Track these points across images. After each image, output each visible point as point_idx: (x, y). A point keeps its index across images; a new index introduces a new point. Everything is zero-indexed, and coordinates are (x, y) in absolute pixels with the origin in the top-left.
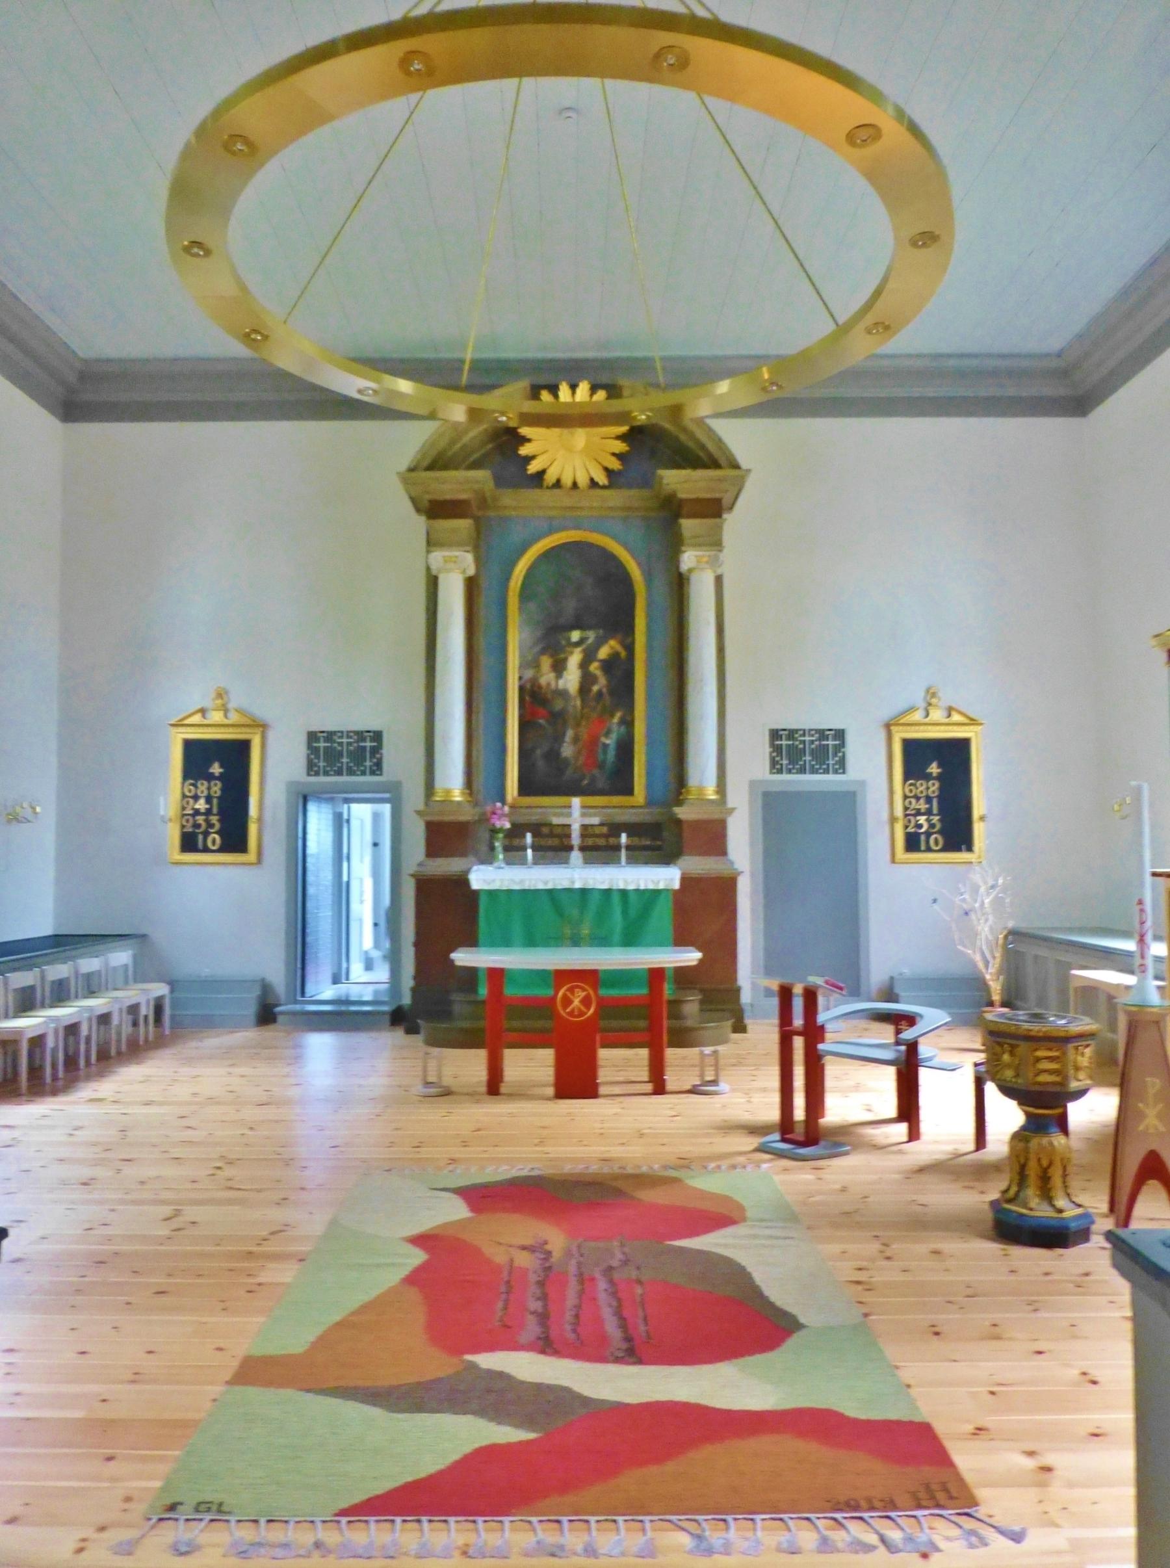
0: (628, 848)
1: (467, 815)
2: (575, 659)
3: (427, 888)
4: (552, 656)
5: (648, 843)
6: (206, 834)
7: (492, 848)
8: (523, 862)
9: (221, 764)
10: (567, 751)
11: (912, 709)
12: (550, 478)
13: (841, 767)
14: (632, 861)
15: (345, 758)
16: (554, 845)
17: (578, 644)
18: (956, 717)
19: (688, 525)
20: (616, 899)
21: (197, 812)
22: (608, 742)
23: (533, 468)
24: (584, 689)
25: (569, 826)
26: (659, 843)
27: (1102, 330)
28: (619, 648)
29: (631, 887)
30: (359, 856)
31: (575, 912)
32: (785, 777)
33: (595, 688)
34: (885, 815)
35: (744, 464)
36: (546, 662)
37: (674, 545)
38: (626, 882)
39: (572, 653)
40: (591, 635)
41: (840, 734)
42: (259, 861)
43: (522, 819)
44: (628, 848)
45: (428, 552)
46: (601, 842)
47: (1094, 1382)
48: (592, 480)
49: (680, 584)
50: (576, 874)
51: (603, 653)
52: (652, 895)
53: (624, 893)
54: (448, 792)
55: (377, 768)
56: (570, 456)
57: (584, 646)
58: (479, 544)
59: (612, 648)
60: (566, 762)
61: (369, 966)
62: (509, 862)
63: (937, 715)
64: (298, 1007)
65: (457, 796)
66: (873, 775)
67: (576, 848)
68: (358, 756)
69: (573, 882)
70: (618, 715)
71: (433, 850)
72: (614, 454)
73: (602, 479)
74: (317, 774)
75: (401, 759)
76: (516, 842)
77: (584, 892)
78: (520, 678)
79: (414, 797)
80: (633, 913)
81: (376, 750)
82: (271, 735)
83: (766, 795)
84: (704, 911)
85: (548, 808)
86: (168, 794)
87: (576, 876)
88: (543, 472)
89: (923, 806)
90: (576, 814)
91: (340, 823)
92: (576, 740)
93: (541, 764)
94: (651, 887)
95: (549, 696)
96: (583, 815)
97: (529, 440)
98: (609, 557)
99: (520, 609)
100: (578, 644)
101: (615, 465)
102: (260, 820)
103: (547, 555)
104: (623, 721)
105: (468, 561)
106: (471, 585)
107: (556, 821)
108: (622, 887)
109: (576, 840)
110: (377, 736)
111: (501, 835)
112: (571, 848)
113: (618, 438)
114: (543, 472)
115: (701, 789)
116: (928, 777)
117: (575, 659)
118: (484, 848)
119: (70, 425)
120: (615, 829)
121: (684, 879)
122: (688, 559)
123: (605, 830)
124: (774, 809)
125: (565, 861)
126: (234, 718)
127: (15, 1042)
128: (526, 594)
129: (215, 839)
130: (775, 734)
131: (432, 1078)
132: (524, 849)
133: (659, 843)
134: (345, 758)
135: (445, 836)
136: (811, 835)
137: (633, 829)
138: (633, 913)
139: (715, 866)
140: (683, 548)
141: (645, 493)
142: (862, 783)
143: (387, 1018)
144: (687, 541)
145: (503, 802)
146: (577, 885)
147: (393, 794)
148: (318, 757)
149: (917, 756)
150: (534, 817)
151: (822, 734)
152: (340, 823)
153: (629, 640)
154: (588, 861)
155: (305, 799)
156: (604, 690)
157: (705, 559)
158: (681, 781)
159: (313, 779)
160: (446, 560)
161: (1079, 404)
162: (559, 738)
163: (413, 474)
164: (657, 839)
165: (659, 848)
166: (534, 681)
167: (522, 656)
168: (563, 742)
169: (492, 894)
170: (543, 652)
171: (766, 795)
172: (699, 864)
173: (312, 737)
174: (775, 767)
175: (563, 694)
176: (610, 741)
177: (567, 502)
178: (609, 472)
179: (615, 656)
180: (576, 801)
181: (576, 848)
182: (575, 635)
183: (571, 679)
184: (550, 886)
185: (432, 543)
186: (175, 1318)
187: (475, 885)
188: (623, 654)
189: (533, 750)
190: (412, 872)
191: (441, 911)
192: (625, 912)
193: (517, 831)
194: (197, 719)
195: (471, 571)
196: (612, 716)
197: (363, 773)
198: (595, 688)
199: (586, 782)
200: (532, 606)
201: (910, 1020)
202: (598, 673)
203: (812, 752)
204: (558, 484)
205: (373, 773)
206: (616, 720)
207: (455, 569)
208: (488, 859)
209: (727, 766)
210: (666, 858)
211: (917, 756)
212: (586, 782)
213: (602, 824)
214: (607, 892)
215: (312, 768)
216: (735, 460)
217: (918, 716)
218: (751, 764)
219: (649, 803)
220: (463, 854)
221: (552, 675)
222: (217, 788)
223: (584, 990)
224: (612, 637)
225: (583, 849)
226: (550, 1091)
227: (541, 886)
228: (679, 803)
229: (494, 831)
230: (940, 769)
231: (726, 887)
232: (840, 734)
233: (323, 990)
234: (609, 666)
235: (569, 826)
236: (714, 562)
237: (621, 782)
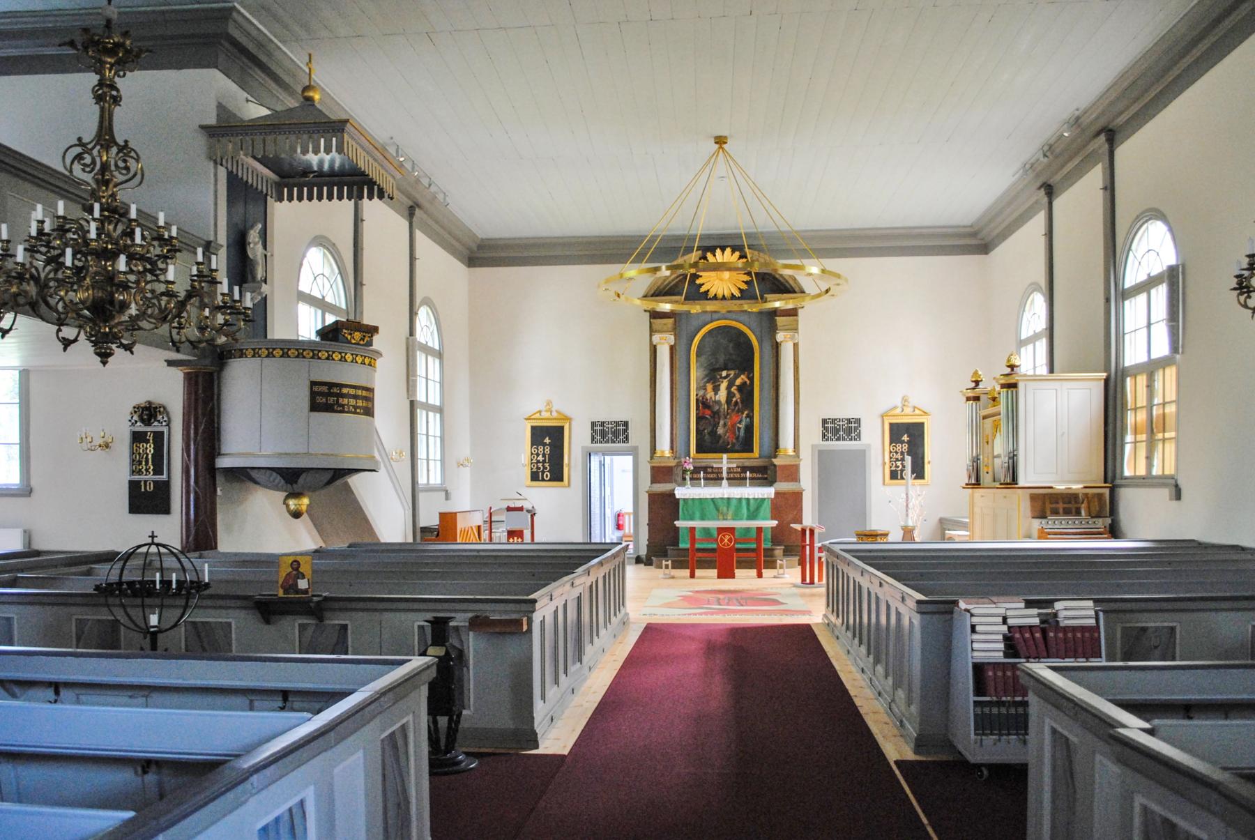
1: (672, 463)
3: (654, 498)
6: (543, 472)
7: (684, 479)
8: (699, 486)
9: (549, 442)
10: (720, 431)
11: (896, 407)
12: (711, 294)
14: (751, 485)
15: (610, 434)
16: (714, 477)
18: (917, 412)
19: (780, 320)
20: (744, 503)
21: (538, 462)
23: (702, 290)
24: (728, 401)
27: (992, 214)
30: (619, 485)
34: (880, 462)
36: (710, 387)
37: (773, 329)
40: (732, 373)
41: (858, 421)
42: (569, 485)
43: (698, 465)
49: (777, 347)
51: (738, 382)
53: (748, 499)
55: (627, 439)
56: (721, 283)
58: (675, 330)
60: (720, 436)
62: (693, 486)
63: (908, 410)
65: (667, 453)
66: (874, 439)
71: (654, 480)
73: (737, 294)
75: (638, 435)
80: (752, 509)
81: (625, 431)
82: (573, 423)
83: (820, 452)
84: (788, 505)
85: (710, 459)
86: (522, 454)
89: (899, 457)
90: (725, 462)
92: (725, 425)
93: (707, 437)
98: (742, 334)
102: (569, 465)
103: (710, 332)
104: (748, 416)
105: (671, 339)
109: (725, 475)
115: (786, 450)
116: (903, 442)
118: (679, 479)
119: (472, 269)
120: (744, 469)
121: (777, 494)
122: (780, 337)
124: (823, 458)
126: (555, 414)
129: (547, 475)
130: (824, 421)
134: (610, 434)
135: (660, 473)
136: (840, 475)
137: (753, 469)
138: (752, 509)
142: (869, 446)
147: (634, 452)
149: (897, 431)
150: (704, 464)
151: (849, 421)
154: (730, 485)
158: (777, 446)
161: (984, 248)
164: (765, 474)
166: (703, 397)
170: (708, 382)
171: (820, 452)
172: (783, 486)
173: (594, 424)
175: (718, 403)
176: (742, 426)
178: (741, 291)
180: (725, 456)
182: (724, 373)
183: (722, 395)
185: (652, 331)
186: (412, 771)
191: (663, 509)
192: (748, 509)
193: (697, 470)
194: (537, 416)
200: (703, 359)
201: (1050, 603)
204: (715, 298)
207: (665, 341)
208: (683, 482)
209: (800, 437)
210: (770, 483)
211: (897, 431)
217: (898, 411)
218: (812, 435)
219: (760, 457)
222: (548, 450)
228: (775, 457)
229: (685, 471)
230: (908, 437)
231: (798, 496)
232: (858, 421)
234: (741, 388)
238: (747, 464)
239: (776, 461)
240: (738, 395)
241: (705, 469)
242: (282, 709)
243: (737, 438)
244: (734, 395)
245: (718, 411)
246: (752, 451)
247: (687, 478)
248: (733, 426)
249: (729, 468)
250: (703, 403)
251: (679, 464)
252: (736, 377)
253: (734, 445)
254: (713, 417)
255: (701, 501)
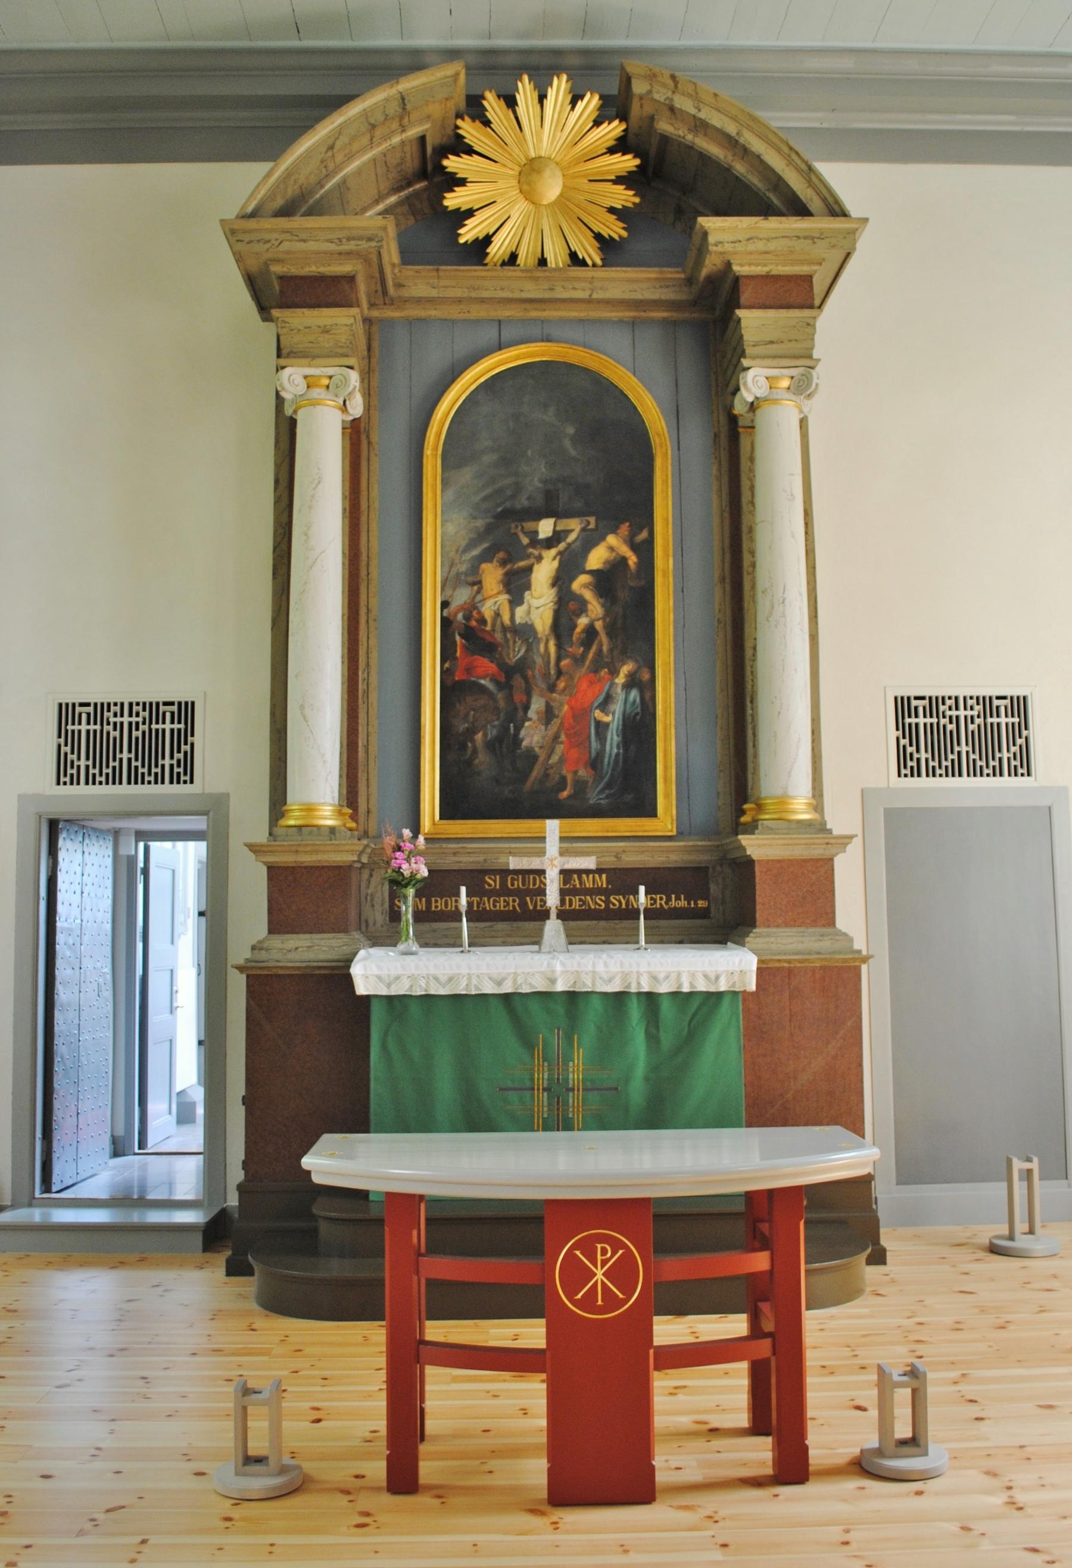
0: (650, 914)
1: (343, 855)
2: (544, 570)
4: (503, 563)
5: (683, 903)
7: (395, 916)
8: (453, 942)
10: (532, 735)
12: (497, 250)
13: (1023, 764)
14: (656, 938)
16: (510, 909)
17: (549, 543)
19: (752, 321)
20: (635, 1012)
22: (607, 719)
23: (468, 233)
24: (561, 626)
25: (541, 872)
26: (701, 904)
28: (625, 551)
29: (663, 988)
31: (556, 1041)
32: (924, 782)
33: (583, 621)
35: (854, 213)
36: (492, 575)
38: (654, 978)
39: (540, 559)
40: (575, 525)
41: (1019, 706)
43: (449, 862)
44: (650, 914)
45: (280, 368)
46: (598, 903)
47: (1020, 1509)
48: (573, 255)
50: (552, 964)
51: (597, 558)
52: (700, 1006)
53: (650, 999)
54: (309, 809)
55: (185, 772)
56: (540, 177)
57: (562, 546)
59: (611, 549)
60: (531, 757)
61: (184, 1116)
62: (426, 942)
64: (36, 1215)
65: (327, 817)
67: (553, 914)
68: (149, 749)
69: (553, 981)
70: (626, 669)
72: (612, 210)
74: (74, 781)
75: (226, 756)
76: (439, 904)
77: (573, 998)
78: (445, 604)
79: (249, 821)
80: (667, 1039)
85: (495, 840)
87: (559, 968)
88: (487, 240)
90: (553, 851)
91: (130, 880)
92: (549, 715)
93: (483, 760)
94: (702, 986)
95: (498, 636)
96: (562, 853)
97: (463, 182)
99: (445, 483)
100: (549, 543)
101: (615, 229)
103: (492, 385)
104: (632, 682)
106: (356, 435)
107: (515, 863)
108: (646, 989)
109: (552, 899)
110: (186, 711)
111: (411, 892)
112: (543, 915)
113: (619, 180)
114: (487, 240)
115: (783, 800)
117: (544, 570)
120: (623, 880)
122: (754, 382)
123: (603, 881)
125: (536, 939)
127: (264, 986)
128: (455, 455)
130: (903, 706)
131: (257, 1446)
132: (456, 916)
133: (701, 904)
135: (305, 892)
137: (658, 880)
138: (667, 1039)
139: (816, 946)
140: (745, 362)
141: (673, 274)
143: (198, 1239)
144: (749, 351)
145: (416, 831)
146: (560, 987)
148: (75, 749)
150: (466, 861)
151: (987, 704)
152: (130, 880)
153: (644, 535)
154: (573, 939)
155: (54, 827)
156: (599, 625)
157: (785, 383)
159: (63, 790)
160: (311, 383)
162: (516, 715)
163: (252, 224)
164: (713, 897)
165: (704, 914)
166: (471, 609)
167: (449, 564)
168: (526, 719)
169: (395, 1003)
170: (486, 556)
172: (783, 941)
173: (66, 713)
174: (907, 765)
175: (526, 632)
176: (613, 718)
177: (532, 290)
178: (604, 243)
179: (618, 565)
180: (553, 827)
181: (553, 914)
182: (545, 528)
183: (539, 605)
184: (507, 988)
187: (361, 989)
188: (632, 560)
189: (471, 732)
190: (241, 962)
192: (653, 1039)
193: (440, 883)
195: (357, 408)
196: (614, 672)
197: (159, 779)
198: (583, 621)
199: (565, 794)
200: (466, 476)
202: (588, 595)
203: (971, 738)
205: (175, 779)
206: (620, 680)
209: (827, 758)
210: (728, 924)
212: (565, 794)
213: (599, 871)
214: (619, 998)
215: (64, 771)
216: (837, 202)
218: (864, 752)
219: (680, 835)
220: (340, 927)
221: (504, 598)
223: (616, 1245)
224: (614, 530)
225: (562, 915)
226: (535, 1472)
227: (489, 989)
228: (738, 828)
229: (398, 883)
232: (1019, 706)
233: (91, 1173)
234: (606, 581)
235: (541, 872)
236: (802, 387)
237: (631, 792)
238: (634, 857)
239: (754, 846)
240: (595, 608)
241: (475, 878)
242: (539, 952)
243: (595, 764)
244: (582, 607)
245: (522, 667)
246: (653, 813)
247: (407, 911)
248: (581, 715)
249: (566, 874)
250: (469, 634)
251: (378, 861)
252: (590, 541)
253: (580, 787)
254: (505, 686)
255: (462, 1005)
